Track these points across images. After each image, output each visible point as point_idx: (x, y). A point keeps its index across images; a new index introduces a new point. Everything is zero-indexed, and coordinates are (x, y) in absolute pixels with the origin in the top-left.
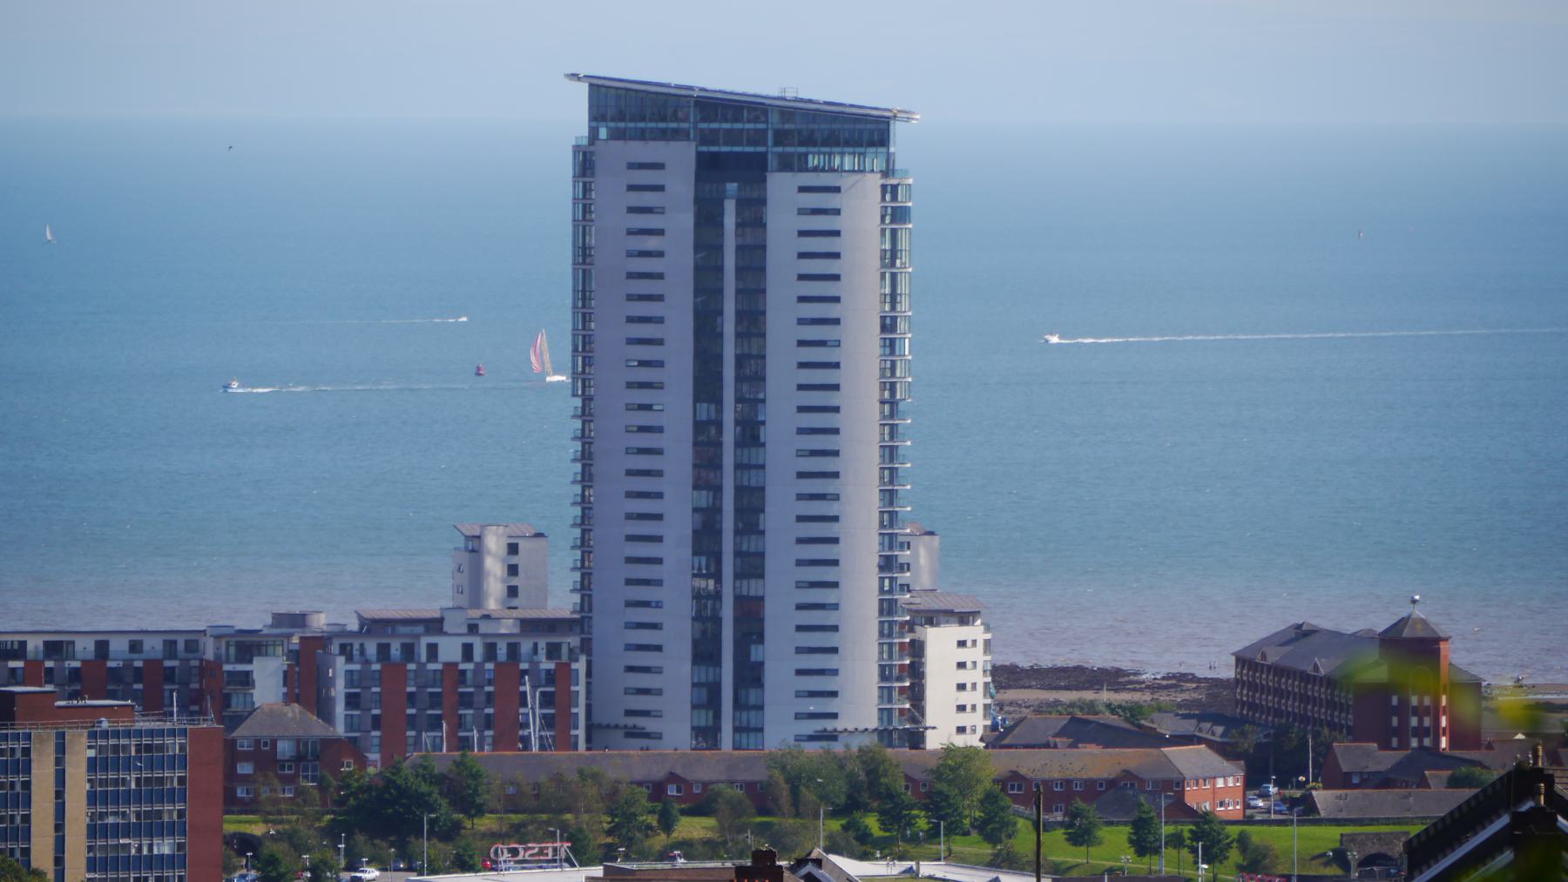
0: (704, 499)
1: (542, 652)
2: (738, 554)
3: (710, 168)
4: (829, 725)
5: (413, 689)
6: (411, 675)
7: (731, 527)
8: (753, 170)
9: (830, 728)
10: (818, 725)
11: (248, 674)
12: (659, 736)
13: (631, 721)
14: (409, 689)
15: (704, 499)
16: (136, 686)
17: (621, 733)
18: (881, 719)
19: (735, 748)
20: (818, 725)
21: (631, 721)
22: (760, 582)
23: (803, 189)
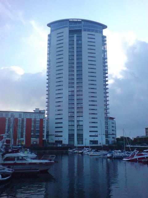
3: (71, 32)
8: (79, 32)
21: (56, 133)
23: (88, 34)
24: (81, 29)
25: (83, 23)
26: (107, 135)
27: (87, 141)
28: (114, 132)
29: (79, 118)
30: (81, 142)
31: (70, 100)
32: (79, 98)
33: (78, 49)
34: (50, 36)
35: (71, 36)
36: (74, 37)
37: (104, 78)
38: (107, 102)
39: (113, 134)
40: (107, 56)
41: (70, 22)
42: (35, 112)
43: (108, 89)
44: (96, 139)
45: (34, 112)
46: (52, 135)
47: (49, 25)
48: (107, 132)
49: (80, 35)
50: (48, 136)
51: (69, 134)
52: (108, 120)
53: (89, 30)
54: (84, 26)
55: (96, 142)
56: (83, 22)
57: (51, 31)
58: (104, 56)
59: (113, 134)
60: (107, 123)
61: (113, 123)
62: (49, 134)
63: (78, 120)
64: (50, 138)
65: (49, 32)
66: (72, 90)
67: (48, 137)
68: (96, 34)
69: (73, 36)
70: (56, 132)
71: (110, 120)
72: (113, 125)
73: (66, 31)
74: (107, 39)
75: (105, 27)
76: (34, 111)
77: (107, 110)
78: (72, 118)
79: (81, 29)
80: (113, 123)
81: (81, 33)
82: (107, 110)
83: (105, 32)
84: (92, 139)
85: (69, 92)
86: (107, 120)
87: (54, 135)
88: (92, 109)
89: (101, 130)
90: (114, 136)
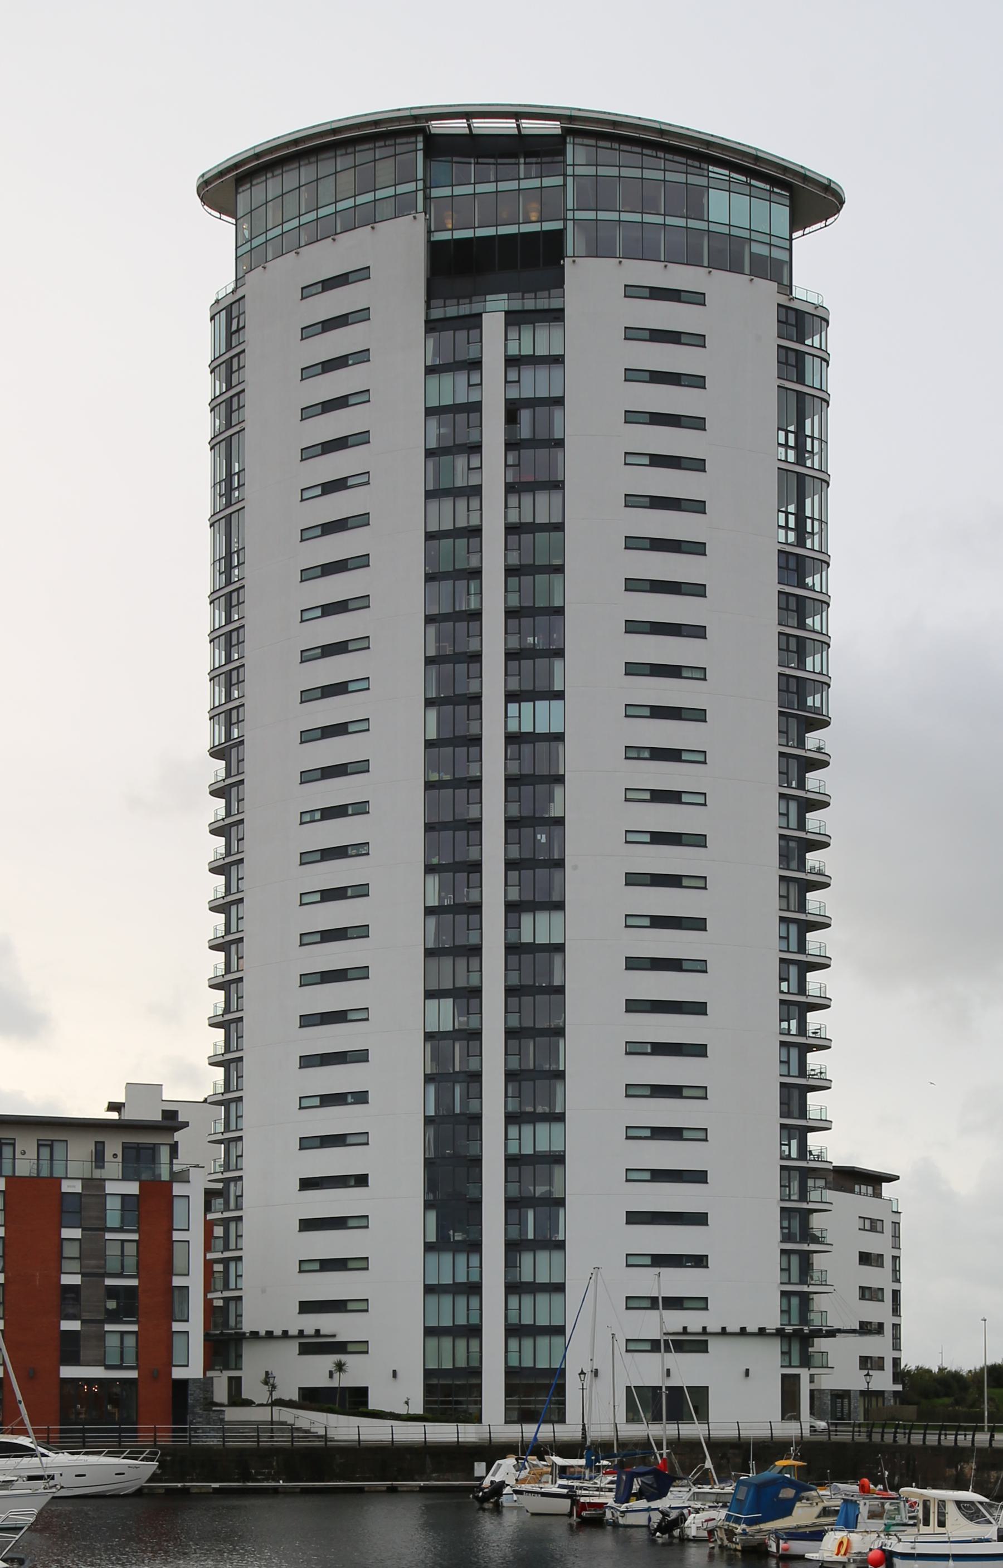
0: (445, 1015)
1: (113, 1167)
2: (513, 949)
3: (457, 270)
4: (692, 1320)
5: (76, 1280)
6: (71, 1251)
7: (494, 831)
8: (531, 263)
9: (695, 1327)
10: (676, 1320)
11: (632, 1417)
12: (362, 1347)
13: (311, 1323)
14: (66, 1280)
15: (445, 1015)
16: (74, 1325)
17: (294, 1346)
18: (785, 1312)
19: (103, 1143)
20: (676, 1320)
21: (311, 1323)
22: (556, 916)
23: (632, 291)
24: (560, 234)
25: (581, 159)
26: (799, 1337)
27: (595, 1409)
28: (878, 1312)
29: (527, 707)
30: (542, 1402)
31: (444, 826)
32: (527, 518)
33: (527, 373)
34: (230, 316)
35: (452, 311)
36: (474, 321)
37: (785, 1018)
38: (810, 976)
39: (866, 1329)
40: (823, 451)
41: (439, 147)
42: (128, 1115)
43: (824, 1126)
44: (686, 1370)
45: (114, 1116)
46: (270, 1335)
47: (225, 188)
48: (798, 1302)
49: (543, 304)
50: (225, 1345)
51: (428, 1373)
52: (814, 1195)
53: (641, 250)
54: (596, 192)
55: (685, 1402)
56: (575, 153)
57: (250, 257)
58: (800, 449)
59: (866, 1329)
60: (798, 1227)
61: (874, 1225)
62: (247, 1327)
63: (513, 727)
64: (254, 1363)
65: (222, 279)
66: (461, 523)
67: (239, 1357)
68: (721, 286)
69: (476, 308)
70: (307, 1307)
71: (830, 1195)
72: (876, 1244)
73: (395, 253)
74: (837, 339)
75: (811, 200)
76: (113, 1107)
77: (812, 1017)
78: (461, 584)
79: (560, 234)
80: (874, 1225)
81: (559, 282)
82: (812, 1017)
83: (819, 262)
84: (649, 1371)
85: (433, 1003)
86: (803, 1197)
87: (285, 1334)
88: (659, 1091)
89: (744, 1286)
90: (876, 1346)
